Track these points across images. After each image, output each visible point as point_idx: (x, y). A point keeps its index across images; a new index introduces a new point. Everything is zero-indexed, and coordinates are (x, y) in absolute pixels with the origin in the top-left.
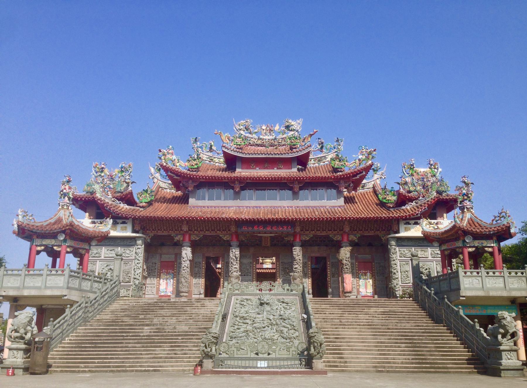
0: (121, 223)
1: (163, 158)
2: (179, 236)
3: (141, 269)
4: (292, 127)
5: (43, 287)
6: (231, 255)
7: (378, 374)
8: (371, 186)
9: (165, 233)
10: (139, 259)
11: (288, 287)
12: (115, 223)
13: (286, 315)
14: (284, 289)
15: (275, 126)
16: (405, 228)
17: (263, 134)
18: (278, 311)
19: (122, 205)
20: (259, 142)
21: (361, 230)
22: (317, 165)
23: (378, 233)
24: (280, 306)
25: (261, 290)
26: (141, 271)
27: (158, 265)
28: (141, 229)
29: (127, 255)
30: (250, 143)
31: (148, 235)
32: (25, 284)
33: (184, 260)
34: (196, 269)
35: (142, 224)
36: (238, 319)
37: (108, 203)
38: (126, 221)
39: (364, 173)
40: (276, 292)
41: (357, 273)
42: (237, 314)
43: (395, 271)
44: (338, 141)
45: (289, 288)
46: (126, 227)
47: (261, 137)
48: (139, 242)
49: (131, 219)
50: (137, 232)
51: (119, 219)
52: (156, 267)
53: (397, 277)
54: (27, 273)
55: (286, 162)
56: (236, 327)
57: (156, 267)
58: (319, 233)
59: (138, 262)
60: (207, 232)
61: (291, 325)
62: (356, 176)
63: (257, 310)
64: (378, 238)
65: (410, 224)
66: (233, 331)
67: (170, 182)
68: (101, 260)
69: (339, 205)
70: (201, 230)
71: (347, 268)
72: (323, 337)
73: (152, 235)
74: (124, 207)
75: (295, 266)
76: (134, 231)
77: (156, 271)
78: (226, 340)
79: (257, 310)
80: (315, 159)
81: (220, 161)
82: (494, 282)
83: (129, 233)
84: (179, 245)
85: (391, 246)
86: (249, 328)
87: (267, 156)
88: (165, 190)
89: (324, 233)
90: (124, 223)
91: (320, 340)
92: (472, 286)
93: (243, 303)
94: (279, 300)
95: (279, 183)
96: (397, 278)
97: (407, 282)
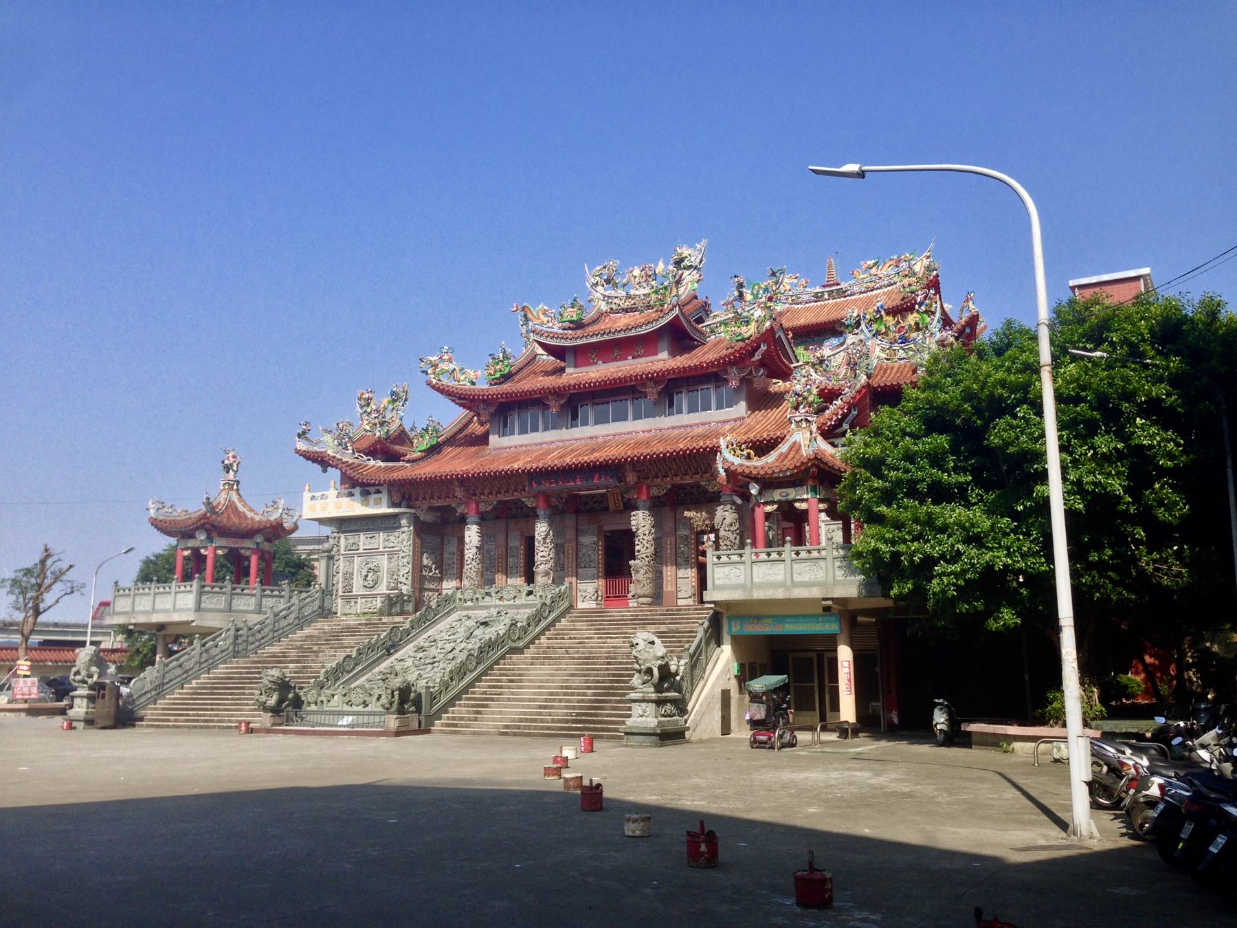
1: (430, 371)
4: (686, 263)
5: (789, 582)
7: (501, 738)
15: (657, 264)
17: (618, 292)
20: (627, 304)
32: (178, 603)
44: (774, 274)
47: (632, 292)
48: (404, 522)
50: (398, 505)
54: (754, 558)
55: (647, 343)
62: (752, 354)
68: (360, 555)
76: (394, 505)
82: (767, 571)
83: (384, 509)
87: (606, 337)
90: (378, 492)
92: (728, 582)
95: (612, 390)
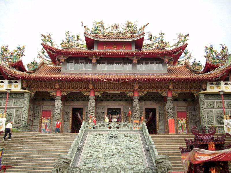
0: (14, 83)
2: (53, 93)
3: (27, 114)
6: (89, 106)
8: (184, 63)
9: (44, 90)
10: (26, 107)
11: (131, 126)
12: (10, 83)
13: (131, 145)
14: (128, 127)
16: (211, 87)
18: (124, 143)
19: (15, 70)
21: (181, 89)
22: (148, 49)
23: (192, 91)
24: (126, 139)
25: (110, 128)
26: (27, 115)
27: (40, 114)
28: (27, 87)
29: (18, 105)
30: (103, 35)
31: (32, 91)
33: (57, 109)
34: (66, 116)
35: (29, 83)
36: (91, 148)
37: (5, 68)
38: (18, 81)
39: (181, 50)
40: (122, 129)
41: (176, 119)
42: (91, 144)
43: (204, 116)
45: (132, 126)
46: (17, 85)
48: (26, 95)
49: (20, 80)
51: (12, 79)
52: (39, 114)
53: (205, 120)
55: (128, 44)
56: (89, 154)
57: (39, 114)
58: (151, 91)
59: (25, 109)
60: (72, 89)
61: (135, 153)
62: (175, 52)
63: (107, 142)
64: (192, 95)
65: (214, 84)
66: (87, 157)
67: (50, 60)
69: (164, 73)
70: (68, 88)
71: (171, 115)
72: (170, 162)
73: (35, 91)
74: (16, 72)
75: (134, 114)
76: (23, 88)
77: (39, 117)
78: (80, 165)
79: (107, 142)
80: (147, 45)
81: (83, 42)
84: (53, 99)
85: (201, 99)
86: (100, 155)
88: (47, 65)
89: (155, 91)
90: (16, 82)
91: (167, 165)
93: (96, 137)
94: (125, 135)
96: (206, 121)
97: (212, 124)
